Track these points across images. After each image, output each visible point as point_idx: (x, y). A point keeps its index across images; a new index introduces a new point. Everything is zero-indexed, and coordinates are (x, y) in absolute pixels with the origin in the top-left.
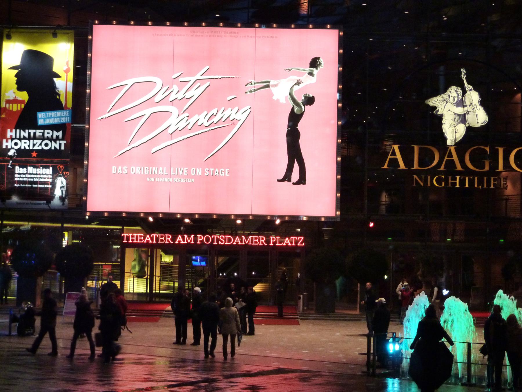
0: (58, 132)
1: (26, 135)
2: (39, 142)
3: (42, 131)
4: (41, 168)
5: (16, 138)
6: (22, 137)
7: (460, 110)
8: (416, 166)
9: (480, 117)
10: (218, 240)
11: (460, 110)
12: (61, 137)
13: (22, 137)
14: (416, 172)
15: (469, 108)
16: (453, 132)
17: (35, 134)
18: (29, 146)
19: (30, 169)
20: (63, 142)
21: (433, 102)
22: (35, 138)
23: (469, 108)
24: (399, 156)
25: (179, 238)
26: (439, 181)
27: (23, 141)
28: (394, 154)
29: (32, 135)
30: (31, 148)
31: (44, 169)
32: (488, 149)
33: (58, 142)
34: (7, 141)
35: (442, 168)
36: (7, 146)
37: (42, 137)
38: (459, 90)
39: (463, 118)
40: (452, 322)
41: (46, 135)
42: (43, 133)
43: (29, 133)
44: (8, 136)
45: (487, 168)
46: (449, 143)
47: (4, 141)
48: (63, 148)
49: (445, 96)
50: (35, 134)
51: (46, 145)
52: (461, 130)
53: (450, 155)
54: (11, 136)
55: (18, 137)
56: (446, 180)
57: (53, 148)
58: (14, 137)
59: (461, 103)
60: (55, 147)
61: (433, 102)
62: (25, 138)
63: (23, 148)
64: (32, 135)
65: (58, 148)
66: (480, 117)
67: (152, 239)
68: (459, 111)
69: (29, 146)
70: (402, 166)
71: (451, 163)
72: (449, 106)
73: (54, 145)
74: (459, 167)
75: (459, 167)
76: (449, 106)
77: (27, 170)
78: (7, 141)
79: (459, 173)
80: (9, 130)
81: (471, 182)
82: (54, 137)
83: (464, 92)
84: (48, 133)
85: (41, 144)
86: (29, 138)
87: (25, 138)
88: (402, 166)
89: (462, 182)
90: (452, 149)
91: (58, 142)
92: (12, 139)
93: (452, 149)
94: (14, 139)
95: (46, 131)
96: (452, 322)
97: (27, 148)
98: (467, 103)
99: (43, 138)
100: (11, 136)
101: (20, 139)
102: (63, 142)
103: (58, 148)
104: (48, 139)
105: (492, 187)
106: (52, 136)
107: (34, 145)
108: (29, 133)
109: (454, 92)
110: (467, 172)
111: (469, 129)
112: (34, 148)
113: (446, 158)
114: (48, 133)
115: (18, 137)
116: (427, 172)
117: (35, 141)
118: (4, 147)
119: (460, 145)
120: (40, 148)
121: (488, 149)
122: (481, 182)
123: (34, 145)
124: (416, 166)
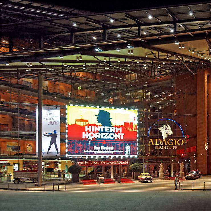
2: (107, 134)
4: (108, 147)
5: (91, 132)
7: (166, 131)
8: (156, 144)
9: (171, 133)
10: (105, 163)
11: (166, 131)
12: (121, 132)
14: (156, 145)
15: (168, 130)
16: (164, 136)
17: (104, 129)
19: (103, 148)
20: (122, 135)
21: (160, 129)
24: (165, 142)
25: (95, 163)
26: (161, 147)
28: (151, 141)
30: (102, 137)
31: (110, 147)
32: (173, 140)
35: (162, 144)
36: (85, 137)
37: (109, 131)
38: (166, 126)
39: (167, 133)
44: (86, 130)
46: (164, 138)
47: (84, 133)
48: (122, 138)
49: (162, 127)
50: (104, 129)
53: (164, 141)
55: (93, 131)
56: (163, 147)
58: (90, 131)
59: (166, 129)
61: (160, 129)
62: (97, 132)
63: (96, 138)
65: (119, 138)
66: (171, 133)
68: (166, 131)
69: (100, 136)
71: (164, 143)
73: (116, 136)
74: (166, 144)
76: (164, 130)
77: (100, 148)
79: (166, 145)
81: (169, 148)
82: (117, 132)
83: (167, 127)
85: (108, 136)
86: (100, 132)
87: (97, 132)
88: (153, 144)
89: (167, 147)
92: (89, 132)
93: (165, 140)
97: (99, 138)
98: (168, 129)
100: (88, 130)
101: (94, 132)
102: (122, 135)
103: (119, 138)
107: (104, 136)
108: (100, 129)
109: (165, 126)
112: (104, 138)
113: (163, 142)
115: (93, 131)
116: (159, 145)
117: (104, 134)
118: (84, 137)
119: (167, 139)
120: (108, 138)
121: (173, 140)
122: (171, 148)
123: (104, 136)
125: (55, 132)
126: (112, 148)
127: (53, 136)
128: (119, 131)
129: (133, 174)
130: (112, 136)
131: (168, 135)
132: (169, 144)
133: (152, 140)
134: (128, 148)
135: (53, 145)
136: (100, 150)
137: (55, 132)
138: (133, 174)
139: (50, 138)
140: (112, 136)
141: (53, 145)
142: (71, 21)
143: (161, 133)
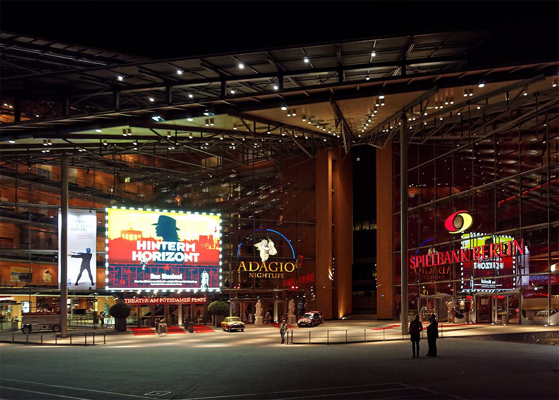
4: (173, 274)
5: (147, 250)
6: (153, 249)
7: (267, 249)
8: (251, 270)
9: (274, 252)
10: (169, 300)
11: (267, 249)
12: (194, 250)
13: (153, 249)
16: (264, 257)
17: (167, 246)
19: (164, 276)
21: (256, 245)
23: (270, 248)
24: (244, 266)
26: (259, 275)
27: (155, 253)
32: (277, 263)
33: (191, 254)
34: (137, 253)
35: (260, 270)
36: (137, 258)
38: (266, 241)
44: (138, 248)
45: (277, 270)
47: (134, 253)
48: (196, 260)
49: (261, 243)
51: (179, 257)
53: (263, 266)
55: (149, 248)
58: (144, 248)
59: (267, 246)
61: (256, 245)
62: (156, 250)
66: (274, 252)
67: (139, 301)
68: (266, 249)
70: (245, 270)
71: (263, 269)
74: (267, 270)
75: (267, 270)
79: (267, 272)
81: (271, 276)
82: (187, 250)
83: (268, 242)
85: (173, 256)
86: (161, 250)
88: (245, 270)
89: (268, 276)
90: (264, 263)
91: (191, 254)
92: (143, 251)
93: (264, 263)
94: (145, 251)
97: (159, 260)
98: (269, 246)
101: (151, 251)
105: (501, 285)
110: (270, 272)
111: (270, 256)
117: (167, 253)
119: (267, 262)
120: (173, 260)
121: (277, 263)
122: (274, 276)
124: (251, 270)
126: (180, 277)
127: (86, 257)
129: (213, 317)
131: (270, 256)
132: (271, 270)
136: (161, 279)
138: (213, 317)
143: (259, 252)
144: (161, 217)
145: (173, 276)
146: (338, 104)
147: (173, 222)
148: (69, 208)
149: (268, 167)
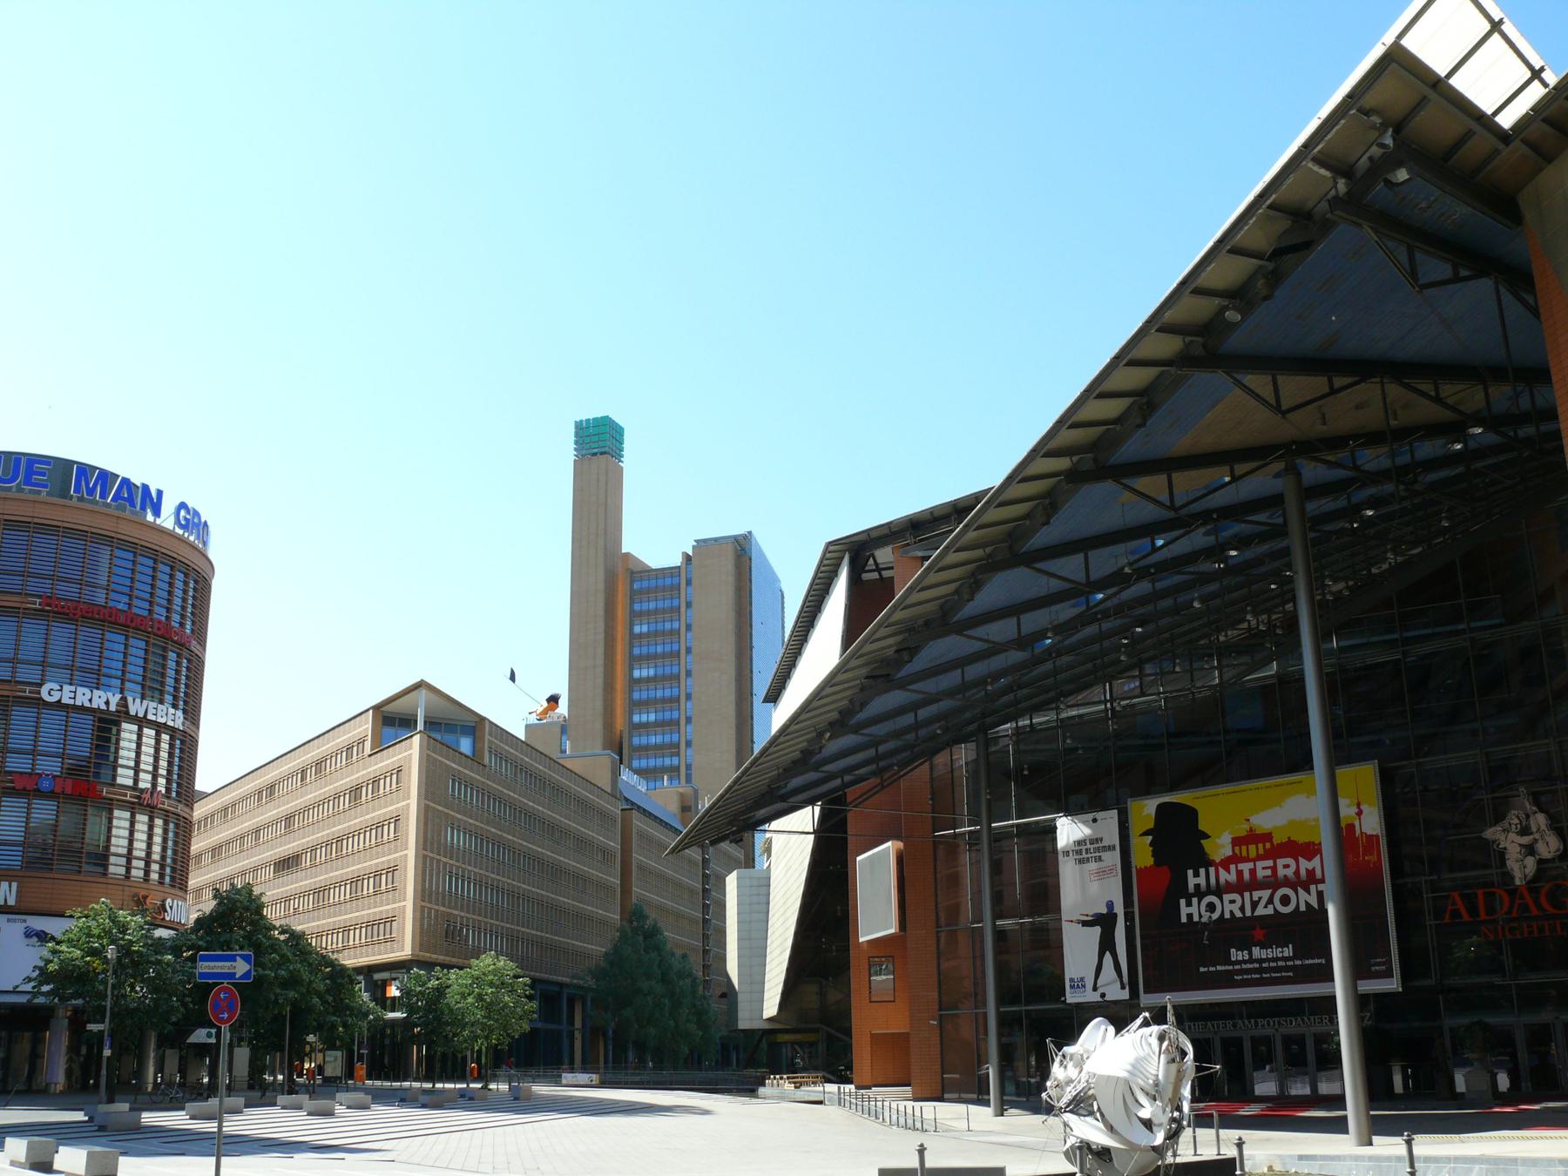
0: (1309, 859)
1: (1232, 877)
2: (1266, 894)
3: (1270, 863)
7: (1526, 840)
11: (1526, 840)
15: (1537, 836)
16: (1521, 869)
17: (1253, 872)
18: (1242, 909)
19: (1257, 952)
21: (1490, 833)
22: (1255, 884)
27: (1227, 897)
29: (1246, 876)
34: (1189, 904)
36: (1190, 916)
39: (1530, 850)
40: (688, 767)
41: (1281, 872)
42: (1274, 869)
43: (1240, 873)
47: (1183, 902)
49: (1505, 823)
50: (1253, 872)
52: (1530, 862)
54: (1197, 886)
57: (1303, 908)
59: (1525, 831)
60: (1307, 903)
61: (1490, 833)
62: (1229, 888)
64: (1246, 876)
69: (1242, 909)
70: (1466, 917)
72: (1512, 836)
76: (1512, 836)
78: (1189, 904)
80: (1190, 872)
84: (1286, 866)
85: (1270, 901)
95: (1281, 862)
96: (688, 767)
98: (1534, 829)
99: (1274, 883)
100: (1197, 886)
101: (1219, 892)
104: (1287, 882)
106: (1297, 872)
107: (1254, 905)
108: (1240, 873)
111: (1541, 862)
112: (1257, 913)
114: (1286, 866)
117: (1256, 895)
118: (1184, 919)
119: (1533, 884)
120: (1270, 911)
123: (1254, 905)
125: (1110, 905)
126: (1288, 951)
127: (1105, 921)
128: (1311, 873)
129: (171, 664)
130: (1285, 900)
131: (1541, 862)
132: (1551, 910)
133: (1458, 899)
134: (93, 1027)
135: (1108, 957)
136: (1251, 961)
137: (1110, 905)
138: (171, 664)
139: (1098, 929)
140: (1285, 900)
141: (1108, 957)
142: (1059, 577)
143: (1502, 855)
144: (1160, 807)
145: (1277, 952)
146: (1185, 500)
147: (1191, 814)
148: (1311, 850)
149: (647, 748)
